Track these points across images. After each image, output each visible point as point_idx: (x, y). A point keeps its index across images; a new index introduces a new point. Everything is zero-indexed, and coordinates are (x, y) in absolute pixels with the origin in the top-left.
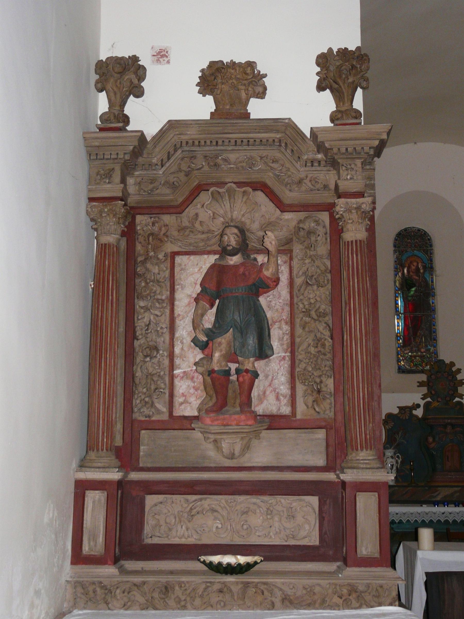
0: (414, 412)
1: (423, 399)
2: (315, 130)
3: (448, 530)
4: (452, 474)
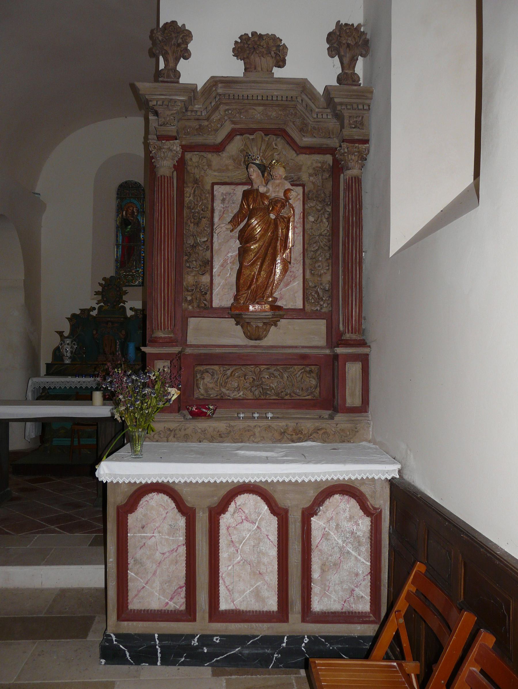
0: (91, 313)
1: (97, 304)
2: (329, 88)
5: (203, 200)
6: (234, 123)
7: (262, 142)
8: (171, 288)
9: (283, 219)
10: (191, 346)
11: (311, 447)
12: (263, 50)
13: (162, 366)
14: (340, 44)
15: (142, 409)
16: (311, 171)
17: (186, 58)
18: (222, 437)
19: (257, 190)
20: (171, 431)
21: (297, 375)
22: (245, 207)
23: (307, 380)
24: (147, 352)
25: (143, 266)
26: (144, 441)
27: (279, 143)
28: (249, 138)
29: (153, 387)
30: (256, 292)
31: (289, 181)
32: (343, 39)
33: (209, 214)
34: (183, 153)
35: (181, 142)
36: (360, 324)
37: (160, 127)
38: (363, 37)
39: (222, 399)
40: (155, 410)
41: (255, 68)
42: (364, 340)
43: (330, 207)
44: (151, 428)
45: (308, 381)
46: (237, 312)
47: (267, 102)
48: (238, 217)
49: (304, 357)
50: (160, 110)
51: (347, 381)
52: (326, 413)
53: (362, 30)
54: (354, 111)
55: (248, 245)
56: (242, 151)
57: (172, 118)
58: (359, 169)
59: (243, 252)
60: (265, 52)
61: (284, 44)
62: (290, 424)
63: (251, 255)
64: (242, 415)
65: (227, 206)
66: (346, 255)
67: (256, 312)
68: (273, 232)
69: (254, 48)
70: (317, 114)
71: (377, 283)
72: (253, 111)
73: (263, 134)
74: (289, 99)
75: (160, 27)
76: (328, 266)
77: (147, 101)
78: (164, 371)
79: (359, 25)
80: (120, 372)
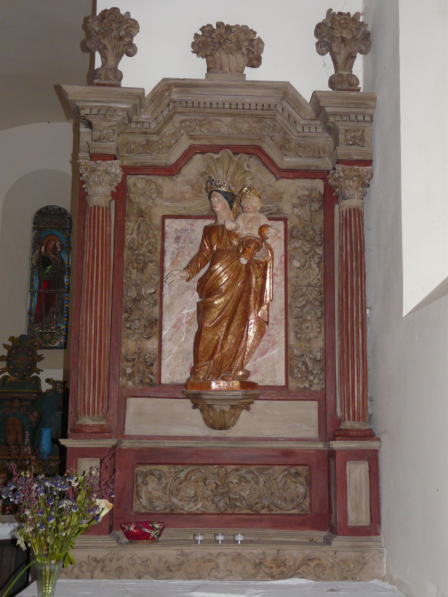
2: (318, 94)
5: (149, 238)
6: (192, 137)
7: (230, 163)
8: (104, 357)
9: (258, 264)
10: (130, 437)
11: (299, 586)
12: (232, 45)
13: (88, 466)
14: (332, 38)
15: (57, 530)
16: (296, 201)
17: (130, 55)
18: (170, 571)
19: (223, 226)
20: (98, 562)
21: (279, 480)
22: (207, 247)
23: (293, 486)
24: (67, 446)
25: (67, 321)
26: (59, 577)
27: (253, 165)
28: (212, 157)
29: (75, 498)
30: (221, 362)
31: (266, 213)
32: (336, 31)
33: (157, 257)
34: (124, 177)
35: (122, 162)
36: (365, 408)
37: (93, 143)
38: (363, 29)
39: (173, 514)
40: (76, 532)
41: (221, 68)
42: (371, 430)
43: (322, 248)
44: (69, 559)
45: (294, 488)
46: (195, 391)
47: (236, 111)
48: (197, 262)
49: (287, 453)
50: (95, 122)
51: (348, 488)
52: (320, 535)
53: (361, 20)
54: (352, 124)
55: (210, 299)
56: (203, 174)
57: (110, 131)
58: (360, 198)
59: (203, 309)
60: (234, 48)
61: (259, 38)
62: (268, 551)
63: (215, 312)
64: (200, 538)
65: (183, 246)
66: (344, 313)
67: (220, 390)
68: (244, 283)
69: (220, 43)
70: (303, 127)
71: (388, 351)
72: (218, 122)
73: (231, 153)
74: (266, 107)
75: (97, 15)
76: (320, 327)
77: (78, 110)
78: (91, 474)
79: (357, 15)
80: (28, 476)
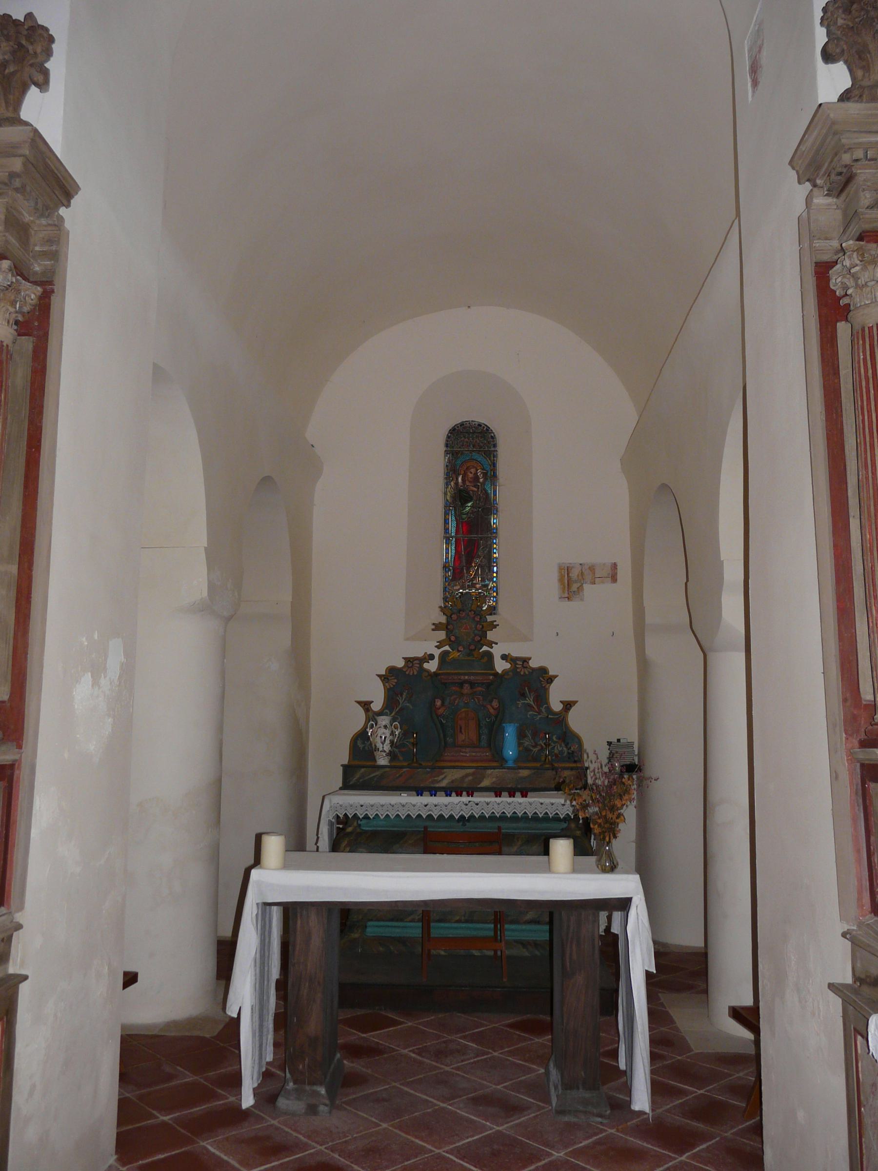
0: (426, 665)
1: (438, 647)
3: (426, 828)
4: (468, 750)
